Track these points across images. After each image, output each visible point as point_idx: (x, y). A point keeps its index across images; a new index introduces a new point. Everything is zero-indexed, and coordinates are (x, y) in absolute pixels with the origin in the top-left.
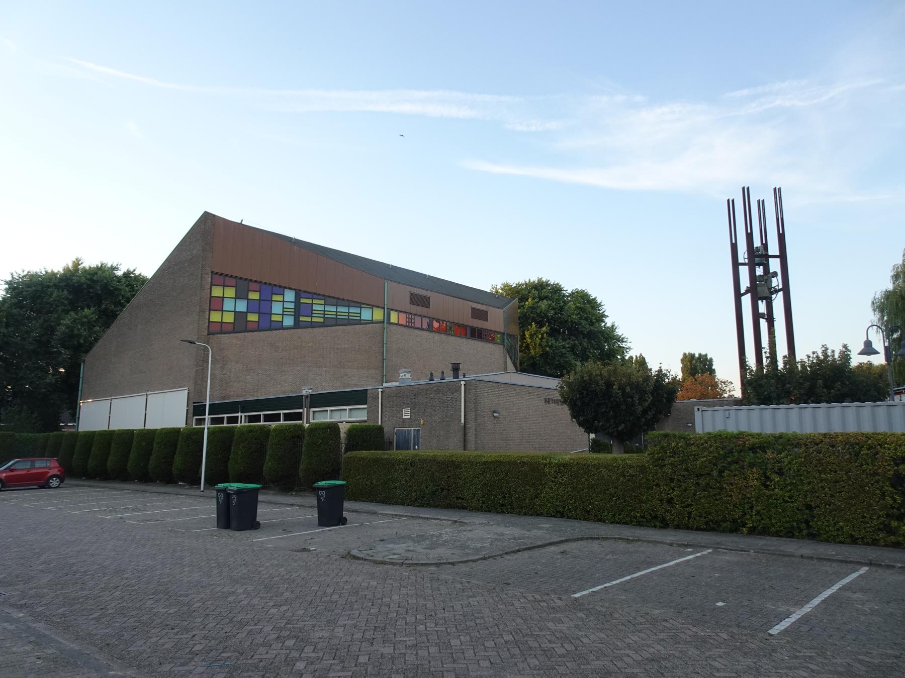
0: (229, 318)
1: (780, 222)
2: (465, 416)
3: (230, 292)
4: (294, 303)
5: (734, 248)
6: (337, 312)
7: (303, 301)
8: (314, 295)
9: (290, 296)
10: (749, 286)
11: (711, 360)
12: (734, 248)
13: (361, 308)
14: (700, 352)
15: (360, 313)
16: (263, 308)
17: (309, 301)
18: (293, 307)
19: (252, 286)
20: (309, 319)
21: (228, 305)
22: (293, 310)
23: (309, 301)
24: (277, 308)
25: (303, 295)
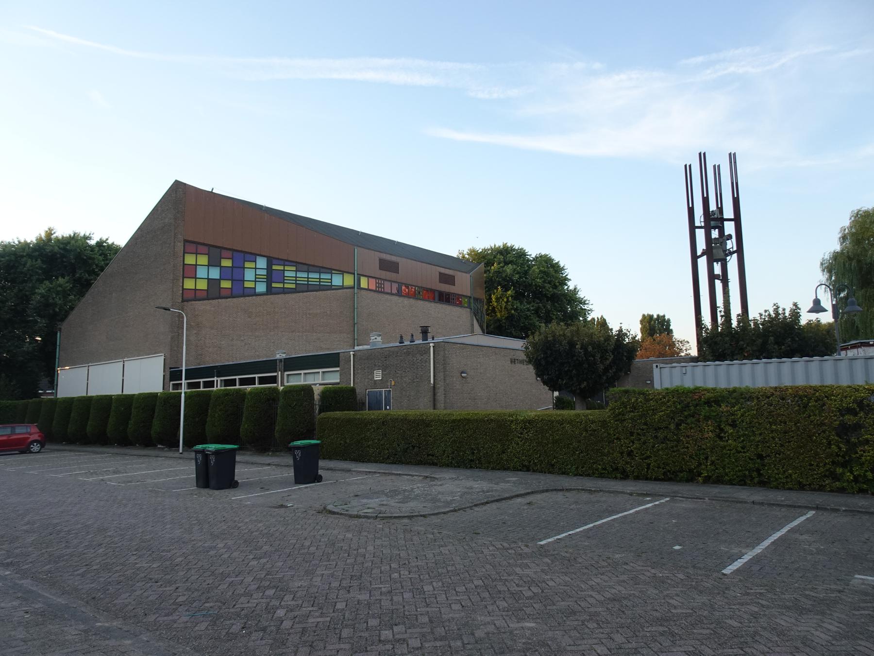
0: (202, 285)
3: (203, 260)
7: (274, 267)
8: (285, 262)
9: (262, 263)
10: (705, 249)
13: (332, 273)
15: (331, 279)
16: (235, 275)
17: (281, 268)
19: (225, 253)
20: (281, 285)
21: (202, 272)
23: (281, 268)
24: (249, 275)
25: (274, 261)
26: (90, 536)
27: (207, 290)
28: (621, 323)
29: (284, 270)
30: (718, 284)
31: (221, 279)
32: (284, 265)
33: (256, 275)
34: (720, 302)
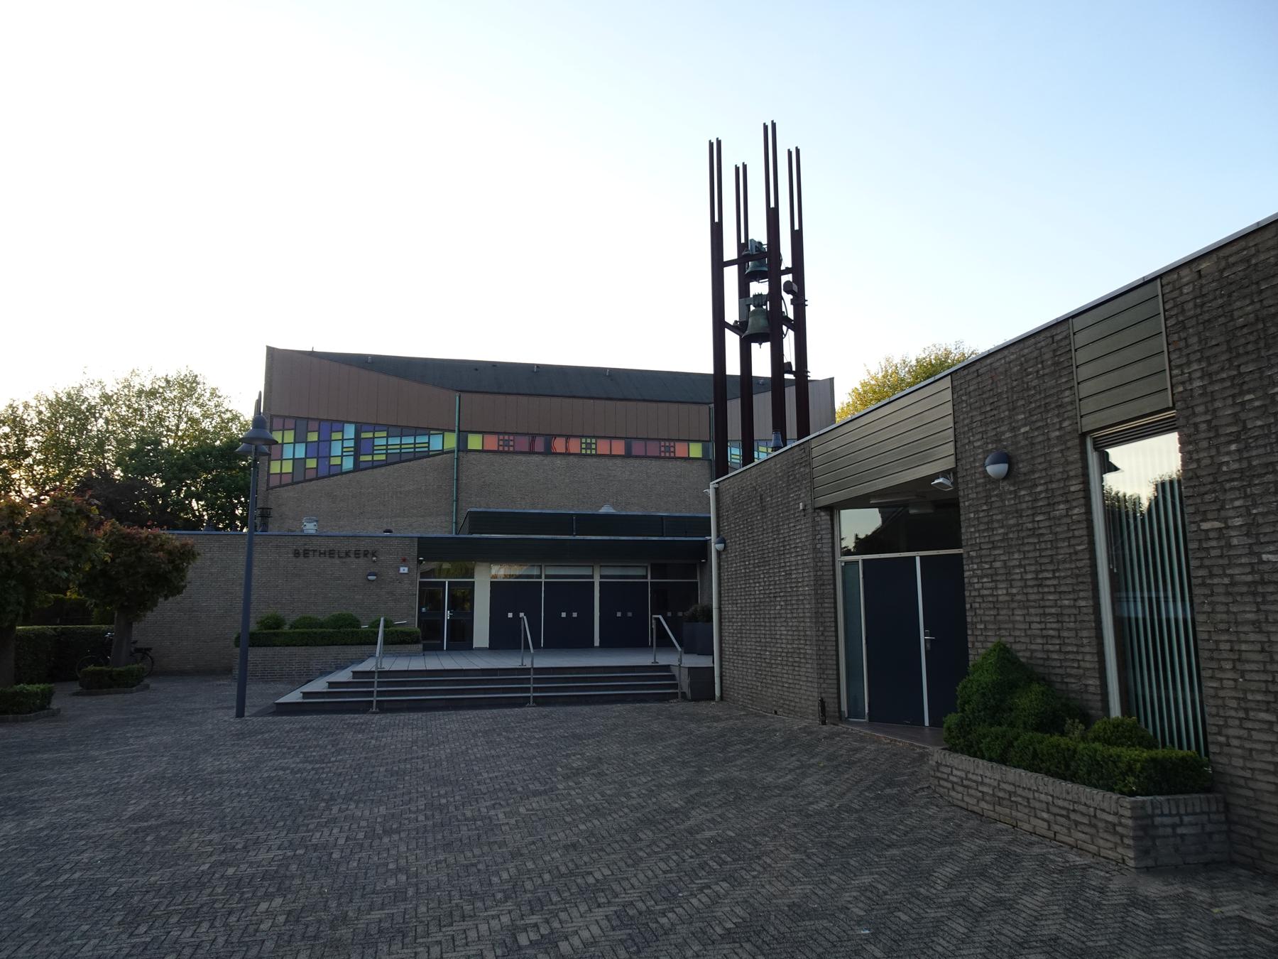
0: (288, 467)
7: (364, 435)
8: (375, 427)
9: (350, 431)
15: (429, 443)
16: (320, 451)
17: (370, 435)
20: (369, 458)
23: (370, 435)
24: (336, 449)
29: (374, 438)
31: (306, 458)
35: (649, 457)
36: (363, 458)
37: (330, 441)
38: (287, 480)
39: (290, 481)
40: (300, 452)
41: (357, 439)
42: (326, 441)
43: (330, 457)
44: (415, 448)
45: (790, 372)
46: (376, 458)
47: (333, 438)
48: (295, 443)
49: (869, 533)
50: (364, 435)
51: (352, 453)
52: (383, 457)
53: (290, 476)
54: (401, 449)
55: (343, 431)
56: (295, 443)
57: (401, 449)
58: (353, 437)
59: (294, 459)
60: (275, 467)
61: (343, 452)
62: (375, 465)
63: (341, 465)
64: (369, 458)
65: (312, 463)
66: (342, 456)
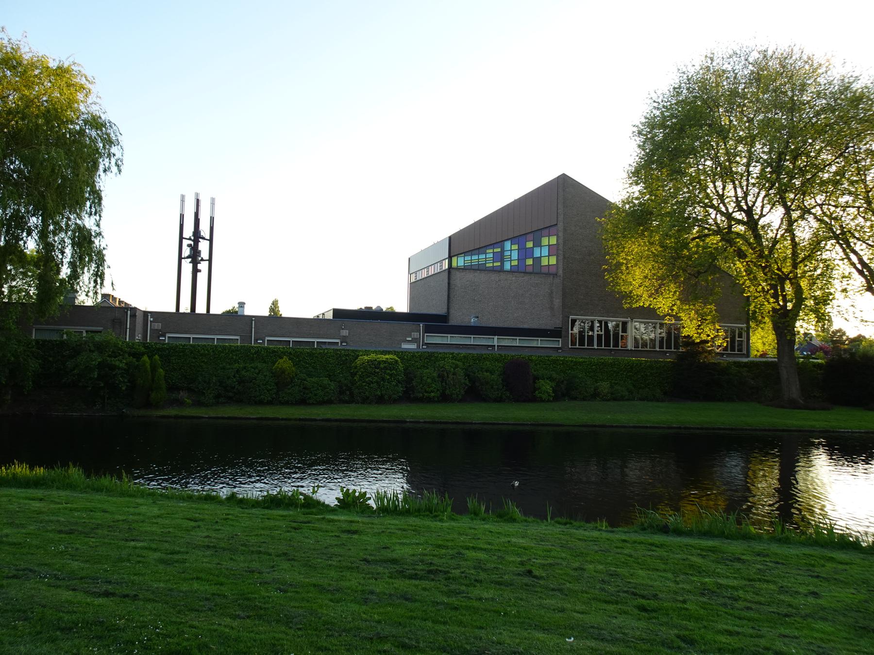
0: (545, 241)
1: (212, 220)
2: (208, 338)
3: (545, 262)
4: (174, 310)
5: (182, 217)
6: (471, 260)
7: (499, 264)
8: (493, 270)
9: (507, 266)
10: (373, 308)
11: (564, 175)
12: (182, 217)
13: (464, 266)
14: (278, 298)
15: (511, 255)
16: (525, 253)
17: (495, 264)
18: (182, 310)
19: (530, 270)
20: (496, 250)
21: (545, 251)
22: (201, 309)
23: (495, 264)
24: (515, 255)
25: (499, 269)
26: (279, 532)
27: (542, 237)
28: (631, 155)
29: (493, 263)
30: (203, 266)
31: (533, 248)
32: (493, 266)
33: (464, 261)
34: (202, 278)
35: (482, 247)
36: (499, 250)
37: (518, 260)
38: (546, 231)
39: (528, 236)
40: (537, 253)
41: (502, 261)
42: (522, 259)
43: (518, 249)
44: (471, 263)
45: (754, 244)
46: (491, 251)
47: (204, 312)
48: (549, 256)
49: (193, 230)
50: (499, 264)
51: (185, 307)
52: (488, 251)
53: (543, 234)
54: (478, 262)
55: (511, 266)
56: (541, 257)
57: (478, 262)
58: (212, 312)
59: (549, 245)
60: (553, 240)
61: (464, 263)
62: (493, 245)
63: (511, 244)
64: (496, 250)
65: (530, 245)
66: (511, 250)
